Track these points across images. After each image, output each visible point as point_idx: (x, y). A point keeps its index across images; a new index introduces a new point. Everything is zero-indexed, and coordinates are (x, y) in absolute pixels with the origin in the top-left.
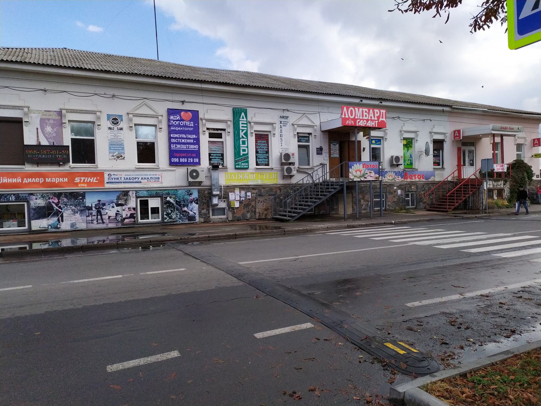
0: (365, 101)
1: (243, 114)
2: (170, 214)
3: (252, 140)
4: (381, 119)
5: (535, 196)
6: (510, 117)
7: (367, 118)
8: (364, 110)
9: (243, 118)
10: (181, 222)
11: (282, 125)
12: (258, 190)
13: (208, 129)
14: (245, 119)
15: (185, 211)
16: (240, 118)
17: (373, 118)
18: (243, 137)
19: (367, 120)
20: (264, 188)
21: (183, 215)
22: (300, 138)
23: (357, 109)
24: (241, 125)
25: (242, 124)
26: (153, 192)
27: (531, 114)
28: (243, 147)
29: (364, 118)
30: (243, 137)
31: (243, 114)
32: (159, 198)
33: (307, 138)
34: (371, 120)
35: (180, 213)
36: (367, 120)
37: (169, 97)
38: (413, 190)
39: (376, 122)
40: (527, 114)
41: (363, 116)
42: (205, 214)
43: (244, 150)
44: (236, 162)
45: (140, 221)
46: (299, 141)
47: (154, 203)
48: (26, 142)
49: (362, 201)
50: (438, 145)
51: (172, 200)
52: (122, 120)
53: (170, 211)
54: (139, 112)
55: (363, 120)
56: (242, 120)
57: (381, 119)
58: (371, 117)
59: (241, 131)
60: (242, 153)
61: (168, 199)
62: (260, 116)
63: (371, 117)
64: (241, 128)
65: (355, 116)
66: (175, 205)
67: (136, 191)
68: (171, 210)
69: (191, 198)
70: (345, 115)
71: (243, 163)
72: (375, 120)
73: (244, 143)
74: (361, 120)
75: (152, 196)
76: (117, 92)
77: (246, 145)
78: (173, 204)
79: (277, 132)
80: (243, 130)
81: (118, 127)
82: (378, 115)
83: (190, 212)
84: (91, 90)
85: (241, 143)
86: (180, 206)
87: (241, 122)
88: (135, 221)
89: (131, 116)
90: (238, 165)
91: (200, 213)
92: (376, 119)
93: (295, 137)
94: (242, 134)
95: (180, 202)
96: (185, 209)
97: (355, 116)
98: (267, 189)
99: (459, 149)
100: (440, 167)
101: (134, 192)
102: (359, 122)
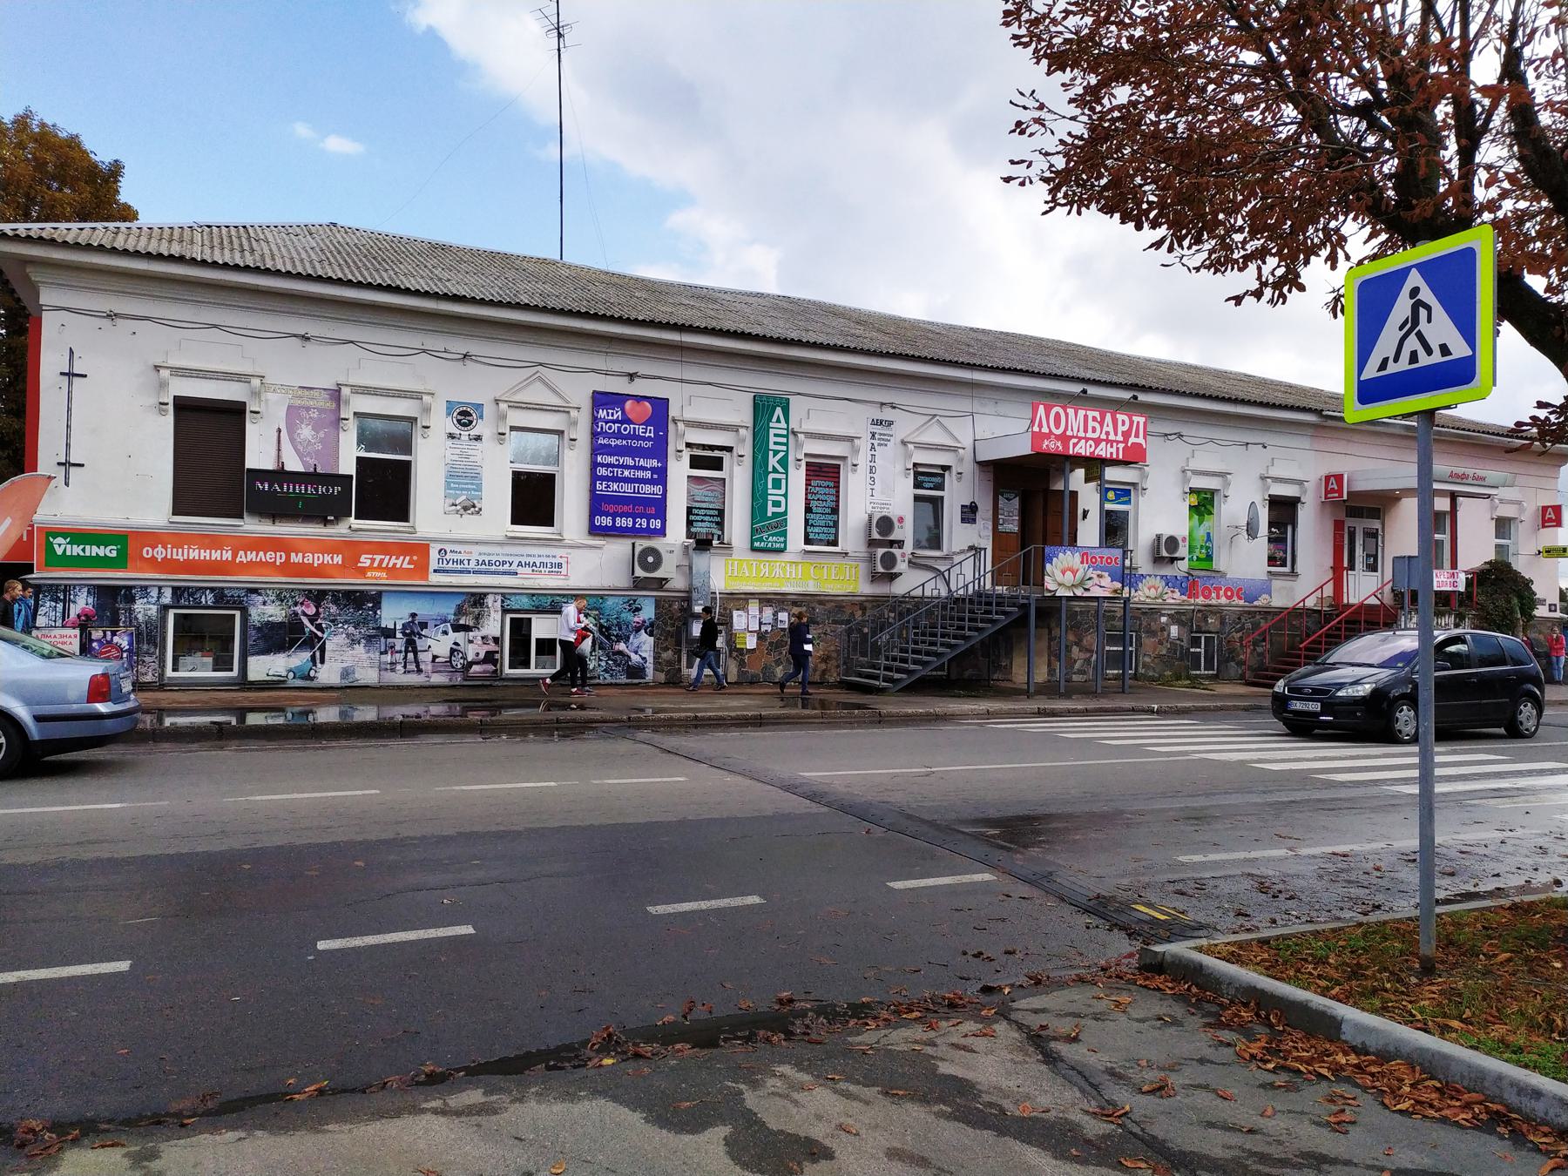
1: (779, 411)
4: (1132, 440)
7: (1096, 436)
8: (1091, 414)
9: (778, 421)
11: (876, 442)
15: (620, 653)
17: (1112, 437)
18: (775, 470)
19: (1098, 441)
22: (921, 478)
23: (1071, 411)
24: (772, 439)
29: (1090, 435)
30: (775, 470)
31: (779, 411)
33: (938, 480)
34: (1107, 441)
36: (1098, 441)
37: (598, 362)
39: (1121, 446)
41: (1086, 431)
42: (669, 663)
43: (777, 504)
44: (754, 531)
45: (507, 671)
46: (917, 485)
50: (1283, 510)
55: (1087, 439)
57: (1132, 440)
60: (771, 510)
62: (822, 417)
63: (1107, 433)
64: (772, 446)
67: (503, 595)
70: (1040, 425)
79: (863, 460)
80: (776, 453)
83: (633, 656)
90: (761, 540)
92: (1120, 438)
94: (773, 461)
95: (608, 629)
96: (622, 646)
98: (829, 606)
99: (1338, 525)
101: (499, 598)
102: (1075, 445)
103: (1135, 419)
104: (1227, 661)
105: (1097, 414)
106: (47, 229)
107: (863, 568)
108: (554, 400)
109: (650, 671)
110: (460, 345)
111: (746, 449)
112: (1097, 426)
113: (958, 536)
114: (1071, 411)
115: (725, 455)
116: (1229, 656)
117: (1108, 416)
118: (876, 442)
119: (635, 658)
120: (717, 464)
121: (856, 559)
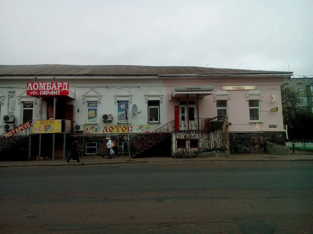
0: (38, 78)
4: (63, 89)
6: (231, 78)
7: (49, 89)
8: (48, 84)
13: (86, 101)
17: (56, 89)
19: (50, 91)
22: (25, 105)
23: (41, 84)
27: (256, 74)
29: (47, 89)
33: (31, 105)
34: (54, 90)
36: (50, 91)
38: (125, 140)
39: (59, 91)
40: (254, 74)
41: (46, 88)
46: (25, 107)
50: (153, 104)
54: (89, 94)
55: (46, 91)
57: (63, 89)
58: (54, 88)
63: (54, 88)
65: (39, 88)
70: (30, 88)
72: (58, 90)
74: (44, 90)
76: (109, 85)
79: (6, 102)
82: (61, 86)
84: (123, 85)
89: (215, 96)
92: (58, 89)
97: (39, 88)
99: (177, 108)
102: (42, 92)
103: (64, 84)
105: (50, 84)
106: (181, 75)
108: (96, 94)
110: (106, 85)
112: (50, 87)
114: (41, 84)
116: (133, 149)
117: (54, 84)
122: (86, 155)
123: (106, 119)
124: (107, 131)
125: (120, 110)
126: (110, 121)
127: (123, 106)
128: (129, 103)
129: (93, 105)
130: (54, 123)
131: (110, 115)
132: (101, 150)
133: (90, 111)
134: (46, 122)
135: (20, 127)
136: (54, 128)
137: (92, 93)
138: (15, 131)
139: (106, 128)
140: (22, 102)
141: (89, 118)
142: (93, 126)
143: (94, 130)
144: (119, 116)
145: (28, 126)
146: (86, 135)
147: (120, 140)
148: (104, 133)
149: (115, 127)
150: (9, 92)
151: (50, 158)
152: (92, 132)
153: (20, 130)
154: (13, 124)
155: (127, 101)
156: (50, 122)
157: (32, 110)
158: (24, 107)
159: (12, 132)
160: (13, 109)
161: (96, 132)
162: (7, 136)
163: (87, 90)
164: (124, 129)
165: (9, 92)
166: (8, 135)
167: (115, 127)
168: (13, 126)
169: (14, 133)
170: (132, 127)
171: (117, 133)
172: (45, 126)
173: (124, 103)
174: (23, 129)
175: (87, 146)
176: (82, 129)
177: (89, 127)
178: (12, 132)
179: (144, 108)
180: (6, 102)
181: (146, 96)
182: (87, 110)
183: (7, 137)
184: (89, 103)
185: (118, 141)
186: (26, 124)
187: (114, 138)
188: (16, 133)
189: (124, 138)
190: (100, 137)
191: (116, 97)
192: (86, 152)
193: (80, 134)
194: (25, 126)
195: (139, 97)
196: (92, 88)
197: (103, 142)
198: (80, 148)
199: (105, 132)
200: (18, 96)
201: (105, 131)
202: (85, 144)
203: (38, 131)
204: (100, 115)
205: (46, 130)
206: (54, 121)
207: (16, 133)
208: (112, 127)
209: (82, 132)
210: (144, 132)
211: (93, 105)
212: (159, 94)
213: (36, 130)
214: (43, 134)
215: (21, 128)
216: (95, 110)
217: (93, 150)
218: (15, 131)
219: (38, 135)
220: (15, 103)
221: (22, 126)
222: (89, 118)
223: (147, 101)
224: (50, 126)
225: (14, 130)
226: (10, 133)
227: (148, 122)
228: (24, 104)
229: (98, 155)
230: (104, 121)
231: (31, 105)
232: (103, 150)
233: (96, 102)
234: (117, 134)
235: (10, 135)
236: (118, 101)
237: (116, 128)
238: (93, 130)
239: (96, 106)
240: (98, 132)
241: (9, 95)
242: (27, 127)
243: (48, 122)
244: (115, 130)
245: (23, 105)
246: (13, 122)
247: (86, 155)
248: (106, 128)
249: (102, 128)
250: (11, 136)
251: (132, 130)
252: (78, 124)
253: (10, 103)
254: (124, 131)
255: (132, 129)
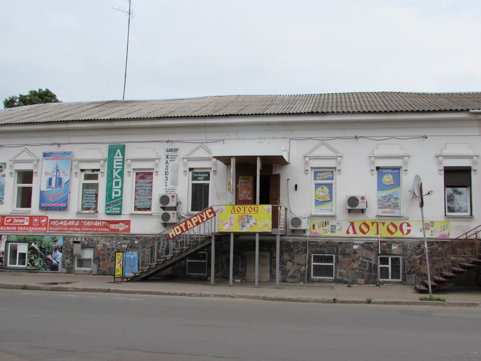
1: (119, 151)
2: (33, 261)
3: (130, 181)
5: (385, 244)
9: (118, 155)
10: (44, 271)
11: (168, 160)
12: (131, 240)
13: (312, 168)
14: (121, 157)
15: (49, 259)
16: (114, 155)
18: (116, 178)
20: (138, 238)
21: (47, 263)
24: (115, 164)
25: (117, 162)
26: (21, 237)
28: (115, 188)
30: (116, 178)
31: (119, 151)
32: (27, 244)
33: (207, 175)
35: (44, 260)
37: (46, 141)
38: (394, 252)
42: (68, 265)
43: (117, 193)
44: (107, 205)
45: (9, 265)
46: (194, 178)
47: (23, 248)
48: (122, 161)
49: (289, 264)
51: (36, 247)
52: (5, 167)
53: (33, 258)
54: (316, 153)
56: (118, 158)
59: (114, 170)
60: (114, 196)
61: (33, 245)
62: (141, 151)
64: (115, 167)
66: (39, 251)
67: (8, 235)
68: (35, 257)
69: (55, 245)
71: (115, 207)
73: (117, 184)
75: (20, 241)
77: (120, 187)
78: (37, 251)
80: (117, 170)
81: (2, 174)
83: (53, 260)
85: (114, 185)
86: (44, 253)
87: (115, 160)
88: (2, 265)
90: (109, 209)
91: (63, 262)
93: (185, 175)
94: (115, 174)
95: (44, 249)
96: (49, 257)
98: (141, 239)
100: (468, 214)
101: (6, 236)
104: (410, 273)
107: (159, 221)
108: (331, 154)
109: (60, 267)
111: (105, 170)
113: (140, 204)
115: (334, 170)
118: (168, 160)
119: (55, 262)
120: (95, 177)
121: (157, 217)
122: (313, 281)
123: (354, 205)
124: (355, 232)
125: (381, 186)
126: (363, 211)
127: (388, 179)
128: (402, 172)
129: (326, 175)
130: (258, 211)
131: (363, 198)
132: (343, 271)
133: (320, 189)
134: (243, 210)
135: (195, 218)
136: (258, 222)
137: (323, 151)
138: (186, 226)
139: (352, 224)
140: (191, 169)
141: (318, 203)
142: (326, 220)
143: (328, 227)
144: (379, 201)
145: (209, 216)
146: (312, 239)
147: (384, 253)
148: (348, 235)
149: (373, 223)
150: (167, 151)
151: (251, 283)
152: (323, 233)
153: (195, 225)
154: (175, 212)
155: (398, 169)
156: (251, 210)
157: (207, 186)
158: (193, 180)
159: (181, 228)
160: (175, 182)
161: (332, 232)
162: (172, 235)
163: (194, 146)
164: (392, 229)
165: (167, 151)
166: (173, 233)
167: (373, 223)
168: (175, 215)
169: (185, 230)
170: (409, 225)
171: (377, 236)
172: (241, 218)
173: (390, 171)
174: (201, 221)
175: (315, 261)
176: (304, 225)
177: (317, 222)
178: (181, 228)
179: (435, 183)
180: (162, 169)
181: (372, 159)
182: (313, 186)
183: (171, 237)
184: (318, 172)
185: (379, 255)
186: (205, 211)
187: (372, 246)
188: (187, 229)
189: (393, 247)
190: (341, 243)
191: (185, 160)
192: (207, 254)
193: (300, 236)
194: (205, 216)
195: (424, 158)
196: (323, 141)
197: (347, 254)
198: (302, 265)
199: (351, 234)
200: (183, 159)
201: (351, 231)
202: (310, 257)
203: (227, 226)
204: (341, 195)
205: (243, 226)
206: (258, 208)
207: (187, 229)
208: (365, 224)
209: (304, 231)
210: (436, 235)
211: (325, 176)
212: (470, 152)
213: (224, 225)
214: (237, 235)
215: (197, 220)
216: (330, 186)
217: (328, 271)
218: (186, 226)
219: (227, 235)
220: (177, 170)
221: (198, 216)
222: (318, 203)
223: (442, 168)
224: (249, 218)
225: (184, 224)
226: (177, 230)
227: (445, 215)
228: (194, 173)
229: (337, 281)
230: (350, 211)
231: (207, 175)
232: (347, 272)
233: (332, 170)
234: (377, 239)
235: (178, 233)
236: (378, 168)
237: (375, 225)
238: (325, 228)
239: (332, 179)
240: (337, 234)
241: (167, 157)
242: (208, 218)
243: (247, 209)
244: (373, 229)
245: (191, 174)
246: (175, 208)
247: (313, 281)
248: (352, 224)
249: (346, 225)
250: (180, 235)
251: (409, 231)
252: (295, 214)
253: (170, 170)
254: (391, 233)
255: (409, 228)
